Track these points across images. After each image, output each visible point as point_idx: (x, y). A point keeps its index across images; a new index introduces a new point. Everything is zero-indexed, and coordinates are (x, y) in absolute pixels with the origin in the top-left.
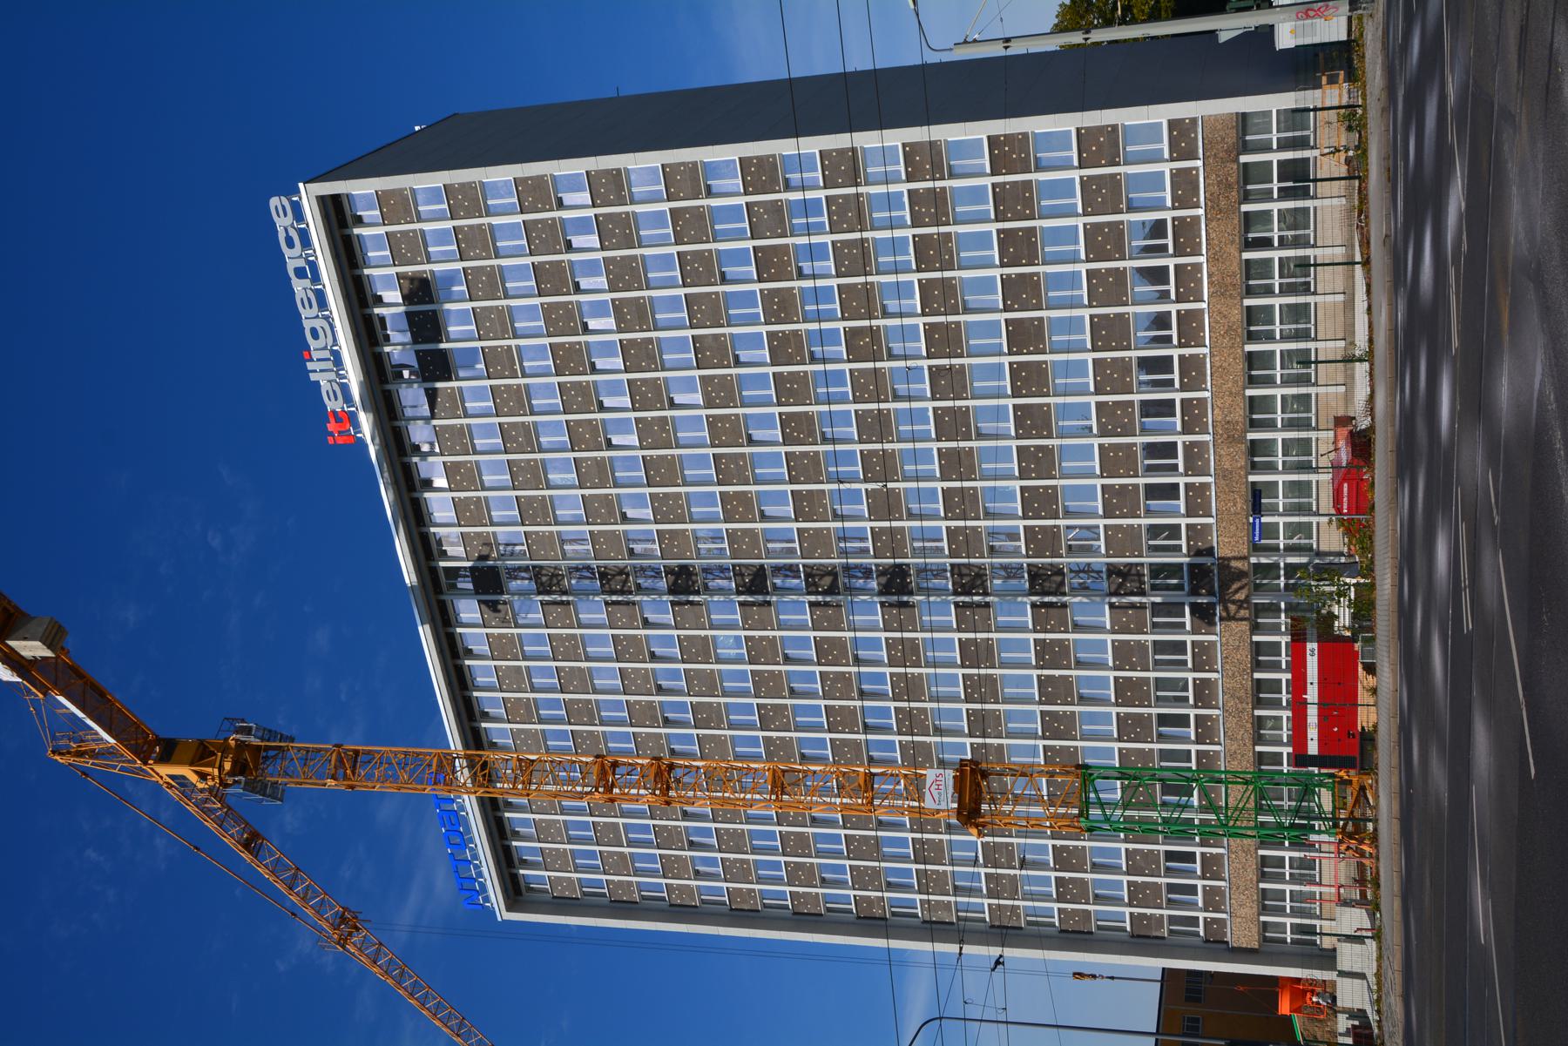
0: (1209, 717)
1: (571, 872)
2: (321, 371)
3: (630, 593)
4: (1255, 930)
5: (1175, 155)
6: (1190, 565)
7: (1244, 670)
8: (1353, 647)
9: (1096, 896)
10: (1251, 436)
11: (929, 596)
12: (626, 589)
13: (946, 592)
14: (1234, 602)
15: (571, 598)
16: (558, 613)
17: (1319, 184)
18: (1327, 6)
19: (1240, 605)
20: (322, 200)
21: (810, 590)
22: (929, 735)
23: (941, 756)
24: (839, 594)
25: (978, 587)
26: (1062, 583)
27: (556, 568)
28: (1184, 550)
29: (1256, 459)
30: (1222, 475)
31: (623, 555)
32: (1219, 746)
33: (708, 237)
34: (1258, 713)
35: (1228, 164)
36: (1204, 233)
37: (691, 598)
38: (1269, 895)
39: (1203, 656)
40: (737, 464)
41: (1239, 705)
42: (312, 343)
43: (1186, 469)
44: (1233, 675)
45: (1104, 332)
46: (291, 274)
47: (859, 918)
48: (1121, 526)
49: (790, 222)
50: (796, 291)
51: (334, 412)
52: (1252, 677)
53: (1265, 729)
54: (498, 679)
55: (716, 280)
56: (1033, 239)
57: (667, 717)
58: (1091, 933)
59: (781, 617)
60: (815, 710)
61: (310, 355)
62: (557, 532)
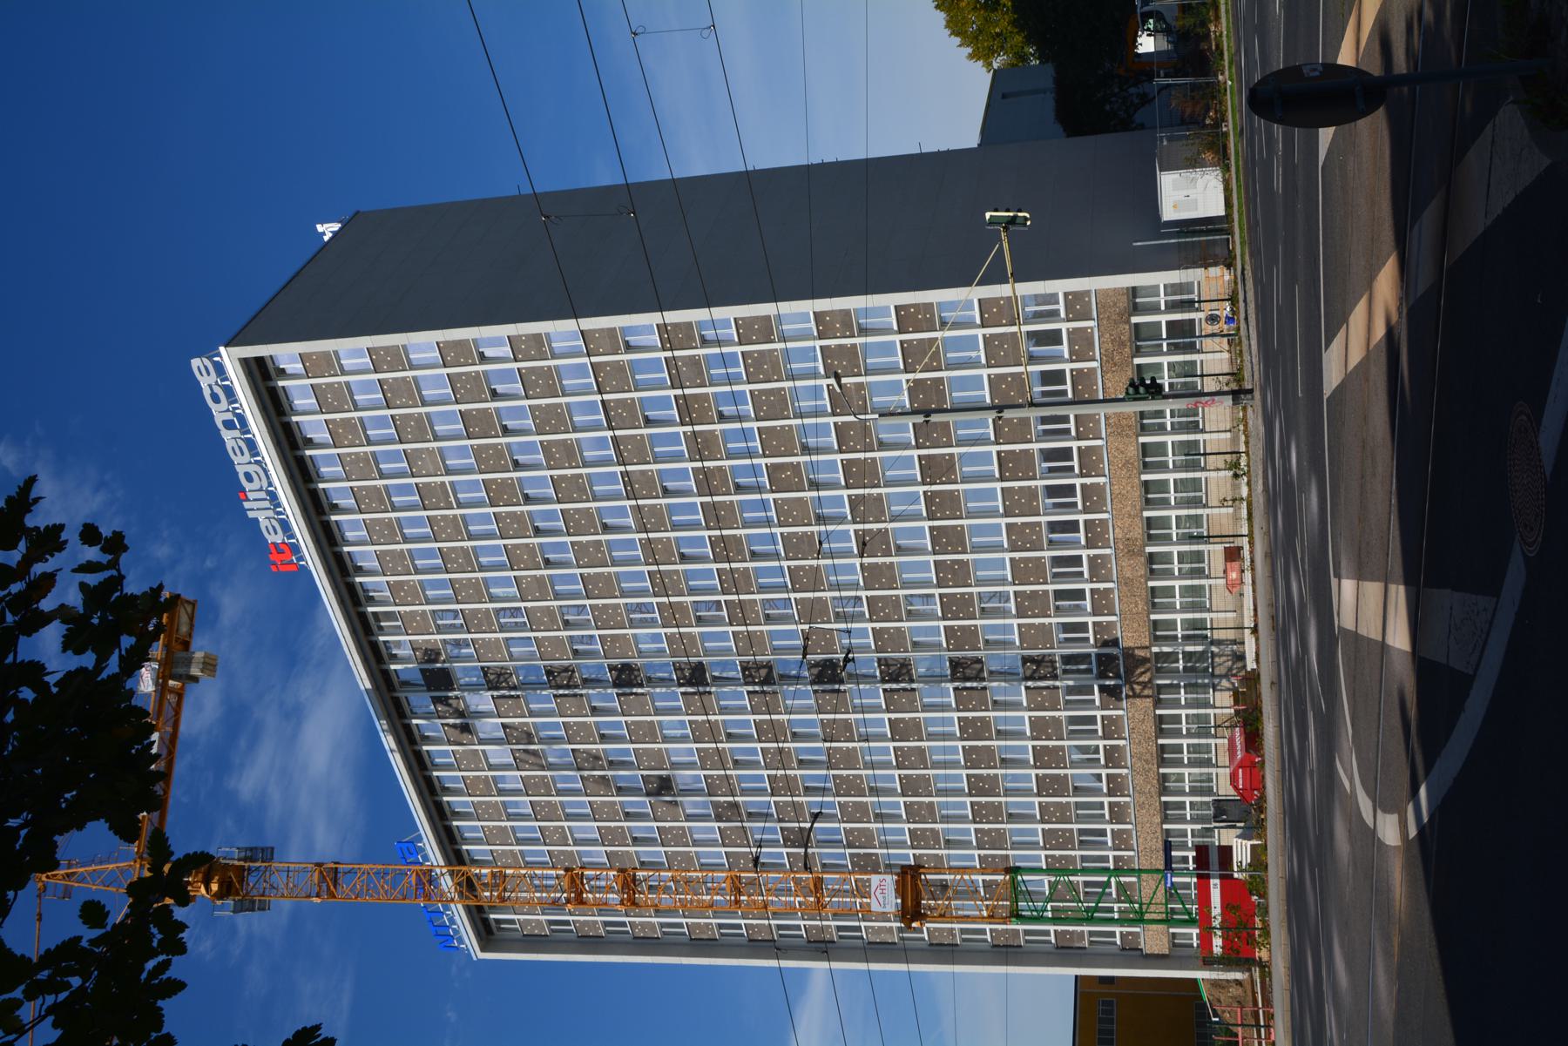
0: (1120, 775)
1: (538, 914)
2: (258, 509)
3: (576, 687)
4: (1165, 940)
5: (1071, 316)
6: (1098, 656)
7: (1149, 738)
8: (1251, 899)
9: (999, 732)
10: (1149, 549)
11: (858, 684)
12: (571, 683)
13: (874, 680)
14: (1138, 683)
15: (519, 693)
16: (509, 705)
17: (1205, 378)
18: (1213, 400)
19: (1145, 685)
20: (245, 363)
21: (747, 680)
22: (865, 796)
23: (804, 440)
24: (774, 684)
25: (904, 674)
26: (982, 670)
27: (502, 668)
28: (1092, 641)
29: (1154, 567)
30: (1124, 582)
31: (567, 654)
32: (1109, 550)
33: (629, 386)
34: (1162, 771)
35: (1121, 326)
36: (1106, 459)
37: (635, 690)
38: (1172, 834)
39: (1111, 728)
40: (671, 579)
41: (1146, 766)
42: (247, 486)
43: (1091, 576)
44: (1140, 742)
45: (1011, 465)
46: (220, 425)
47: (809, 942)
48: (1034, 624)
49: (708, 372)
50: (718, 433)
51: (274, 544)
52: (1156, 743)
53: (1169, 782)
54: (331, 435)
55: (640, 424)
56: (941, 387)
57: (537, 527)
58: (1021, 946)
59: (637, 377)
60: (707, 574)
61: (246, 495)
62: (425, 413)
